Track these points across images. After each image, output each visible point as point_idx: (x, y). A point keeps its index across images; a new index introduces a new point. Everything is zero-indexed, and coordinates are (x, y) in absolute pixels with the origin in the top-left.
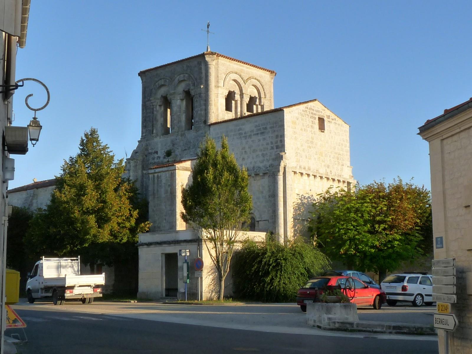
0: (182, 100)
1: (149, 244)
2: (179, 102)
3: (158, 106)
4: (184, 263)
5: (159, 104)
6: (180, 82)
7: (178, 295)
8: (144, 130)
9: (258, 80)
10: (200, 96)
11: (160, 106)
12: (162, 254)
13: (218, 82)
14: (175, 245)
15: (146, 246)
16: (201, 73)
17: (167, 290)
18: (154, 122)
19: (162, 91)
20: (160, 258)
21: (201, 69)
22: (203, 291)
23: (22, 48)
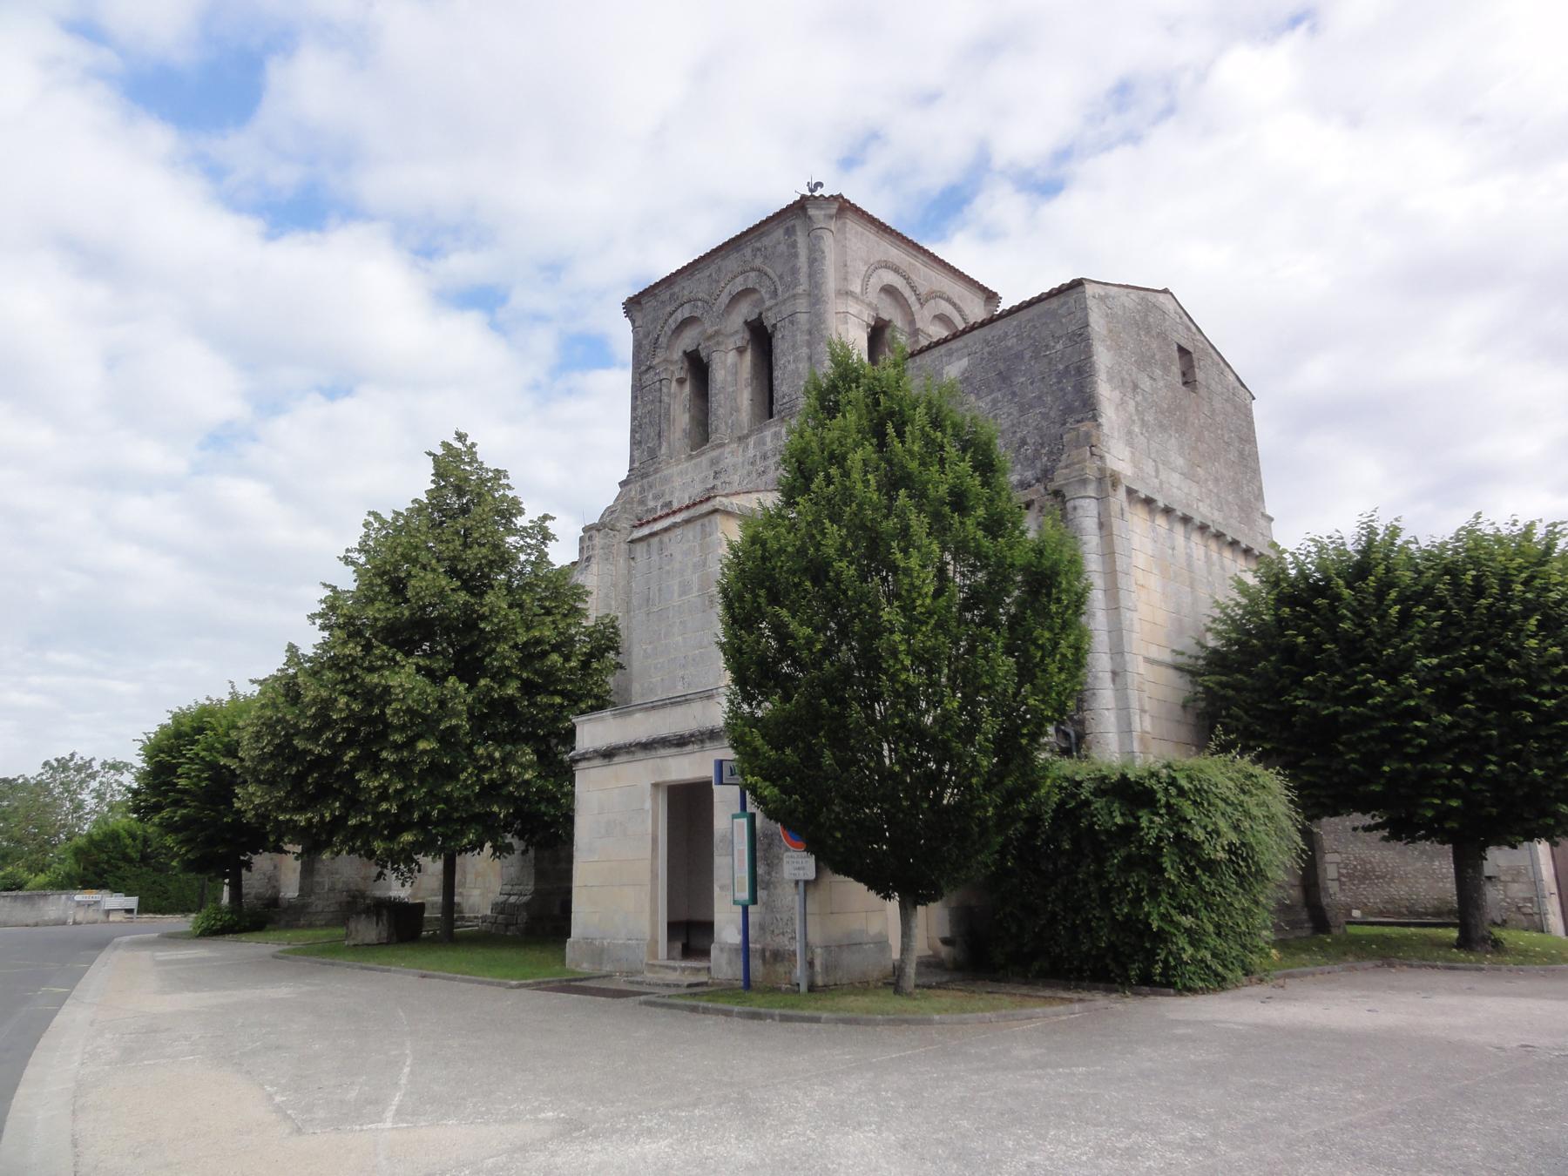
0: (741, 351)
1: (608, 754)
2: (732, 357)
3: (674, 384)
4: (734, 816)
5: (677, 375)
6: (736, 299)
7: (714, 951)
8: (637, 454)
9: (954, 305)
10: (792, 323)
11: (681, 381)
12: (656, 786)
13: (845, 279)
14: (702, 749)
15: (597, 762)
16: (796, 255)
17: (674, 928)
18: (664, 426)
19: (688, 340)
20: (648, 805)
21: (794, 245)
22: (619, 381)
23: (461, 437)
